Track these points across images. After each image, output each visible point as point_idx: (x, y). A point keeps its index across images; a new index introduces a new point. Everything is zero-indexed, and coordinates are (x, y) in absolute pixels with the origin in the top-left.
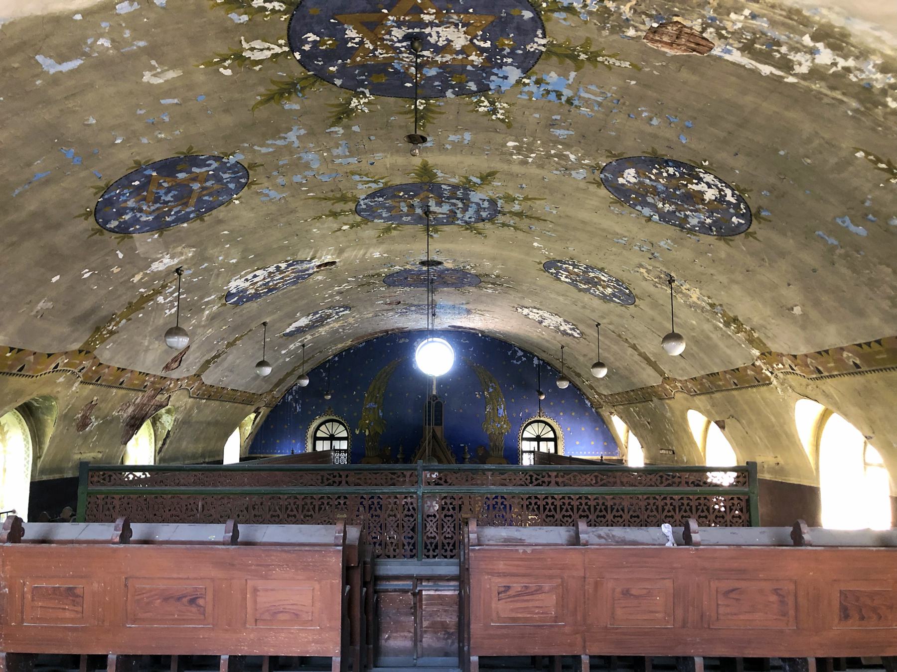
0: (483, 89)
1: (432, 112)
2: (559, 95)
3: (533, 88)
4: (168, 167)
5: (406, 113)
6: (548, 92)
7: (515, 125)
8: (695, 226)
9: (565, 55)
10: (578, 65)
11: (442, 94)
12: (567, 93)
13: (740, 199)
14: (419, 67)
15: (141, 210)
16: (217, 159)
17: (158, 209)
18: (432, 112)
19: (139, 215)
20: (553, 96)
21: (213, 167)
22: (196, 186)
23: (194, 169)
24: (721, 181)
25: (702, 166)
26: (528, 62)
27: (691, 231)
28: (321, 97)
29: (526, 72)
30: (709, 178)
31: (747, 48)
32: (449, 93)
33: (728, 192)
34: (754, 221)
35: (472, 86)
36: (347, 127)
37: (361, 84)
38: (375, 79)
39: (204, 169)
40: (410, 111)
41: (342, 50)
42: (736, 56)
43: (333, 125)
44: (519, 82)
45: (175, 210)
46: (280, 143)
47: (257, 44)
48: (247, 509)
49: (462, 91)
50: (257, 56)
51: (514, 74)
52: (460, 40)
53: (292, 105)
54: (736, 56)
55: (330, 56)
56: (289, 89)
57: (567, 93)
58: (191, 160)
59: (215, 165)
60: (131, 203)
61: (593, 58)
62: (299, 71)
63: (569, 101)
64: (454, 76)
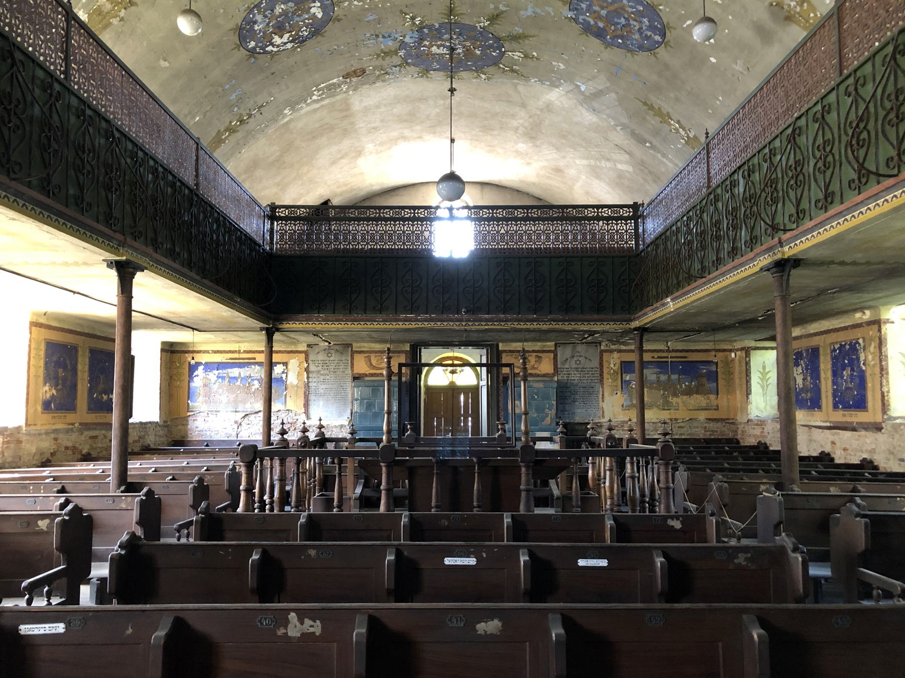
0: (420, 29)
1: (445, 14)
2: (384, 37)
3: (396, 36)
4: (600, 34)
5: (461, 14)
6: (389, 37)
7: (398, 13)
8: (254, 16)
9: (387, 54)
10: (382, 51)
11: (441, 25)
12: (381, 39)
13: (266, 52)
14: (451, 38)
15: (640, 29)
16: (576, 20)
17: (635, 20)
18: (445, 14)
19: (644, 28)
20: (386, 35)
21: (583, 17)
22: (604, 13)
23: (592, 22)
24: (284, 50)
25: (298, 47)
26: (403, 45)
27: (251, 11)
28: (501, 30)
29: (402, 42)
30: (289, 46)
31: (334, 84)
32: (437, 26)
33: (275, 49)
34: (248, 53)
35: (426, 31)
36: (496, 8)
37: (481, 33)
38: (473, 34)
39: (588, 19)
40: (458, 15)
41: (484, 48)
42: (335, 81)
43: (502, 12)
44: (405, 37)
45: (630, 10)
46: (539, 11)
47: (516, 57)
48: (242, 121)
49: (430, 27)
50: (518, 54)
51: (407, 40)
52: (434, 49)
53: (518, 30)
54: (335, 81)
55: (491, 46)
56: (516, 38)
57: (381, 39)
58: (587, 29)
59: (581, 17)
60: (637, 36)
61: (378, 55)
62: (506, 45)
63: (377, 36)
64: (436, 34)
